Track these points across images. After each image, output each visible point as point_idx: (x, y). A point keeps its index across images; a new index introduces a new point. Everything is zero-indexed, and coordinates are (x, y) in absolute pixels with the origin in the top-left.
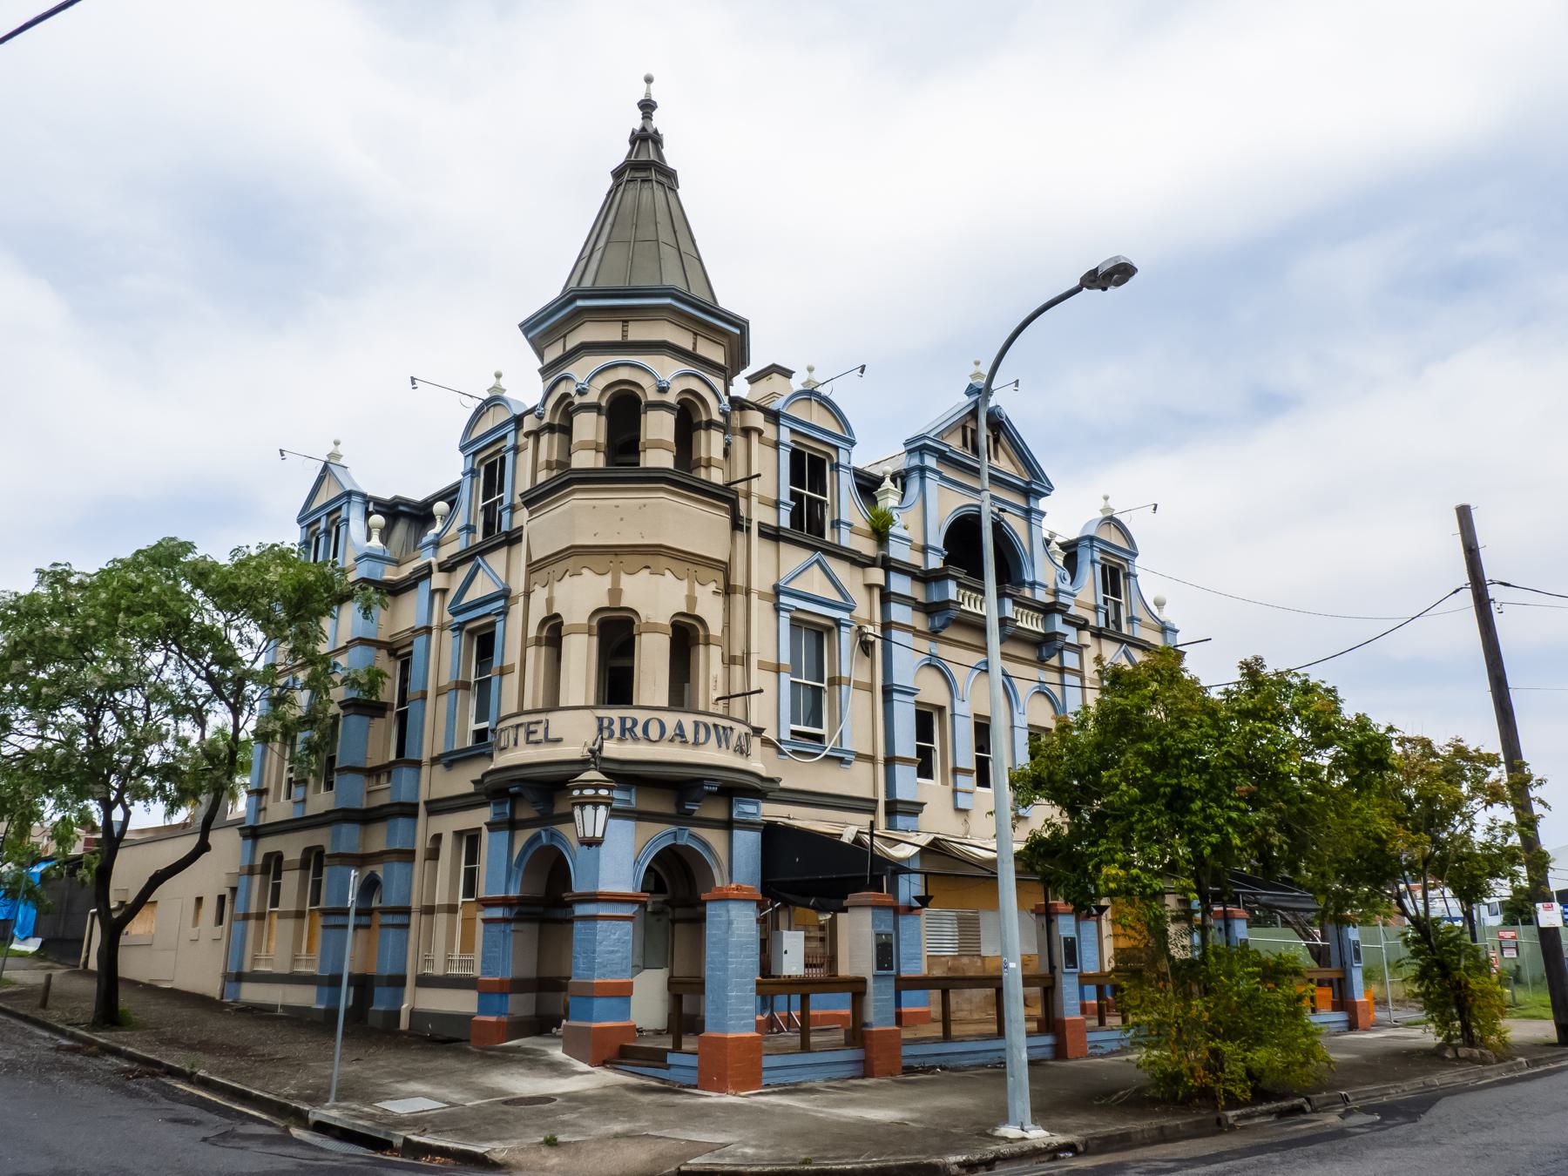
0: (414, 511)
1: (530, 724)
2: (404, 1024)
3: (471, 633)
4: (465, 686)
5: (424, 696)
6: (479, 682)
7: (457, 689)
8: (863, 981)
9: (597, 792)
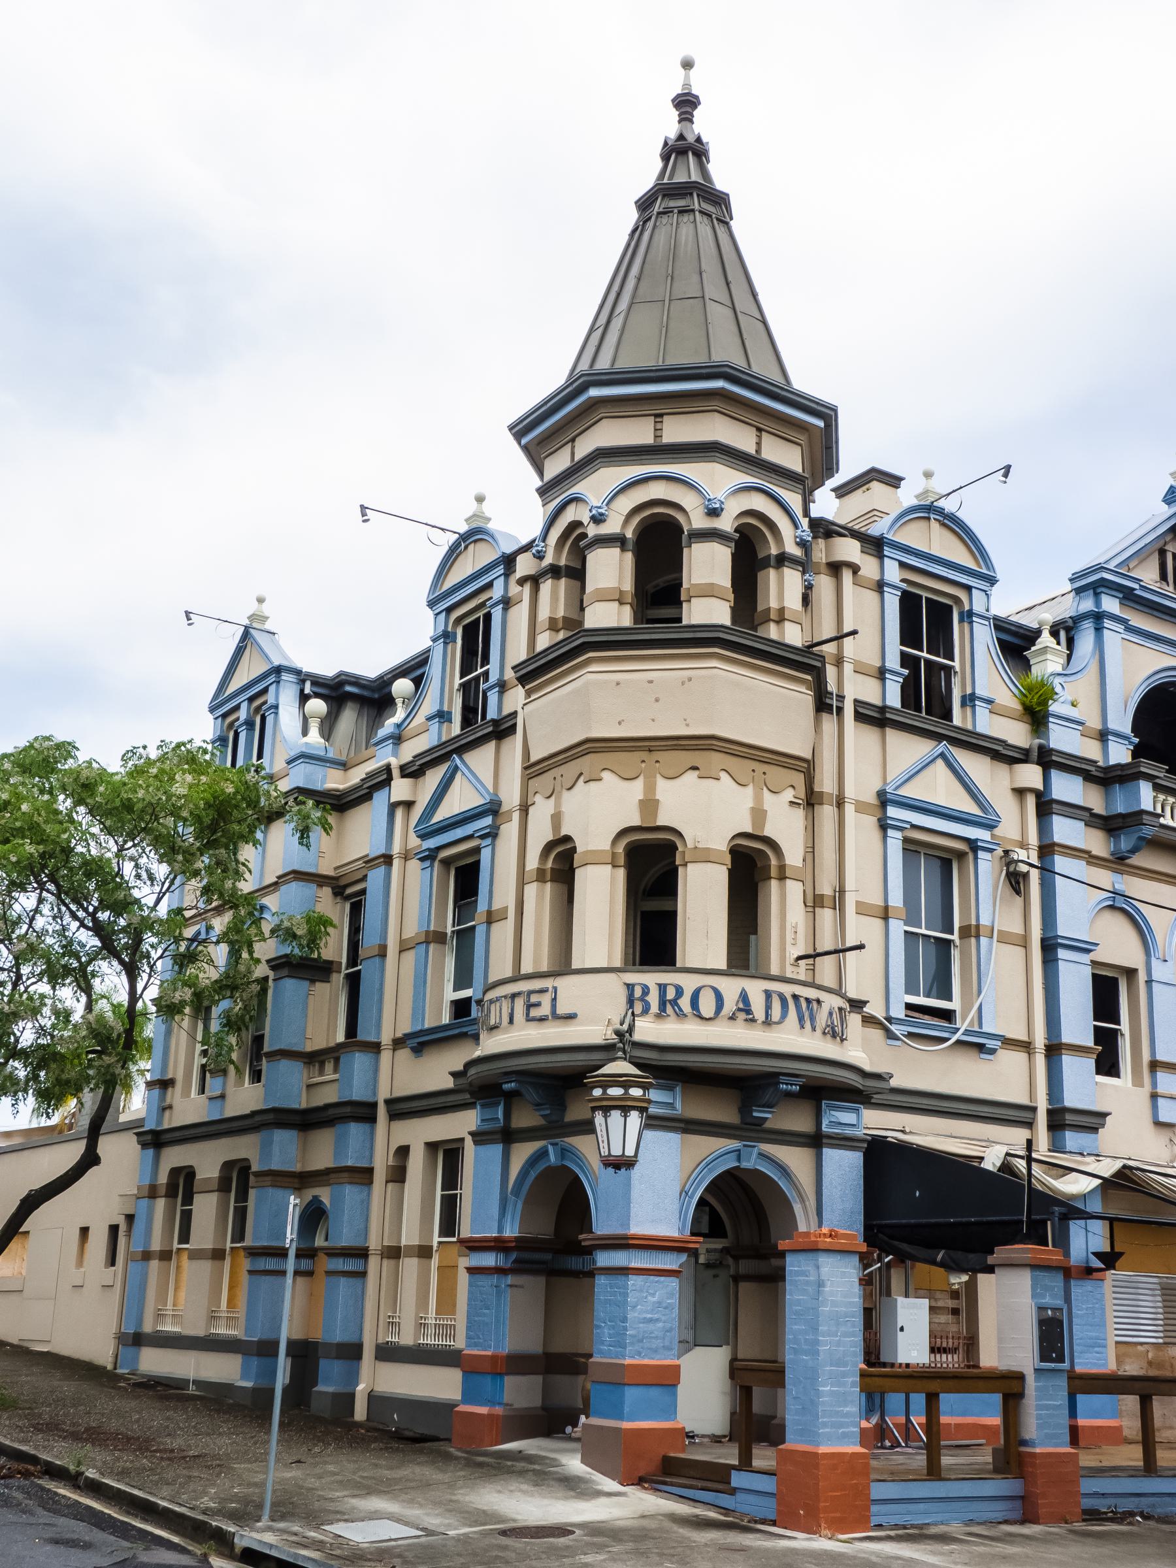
0: (366, 693)
1: (530, 992)
2: (360, 1412)
3: (446, 863)
4: (439, 938)
5: (382, 953)
6: (459, 933)
7: (427, 942)
8: (1020, 1377)
9: (604, 1092)
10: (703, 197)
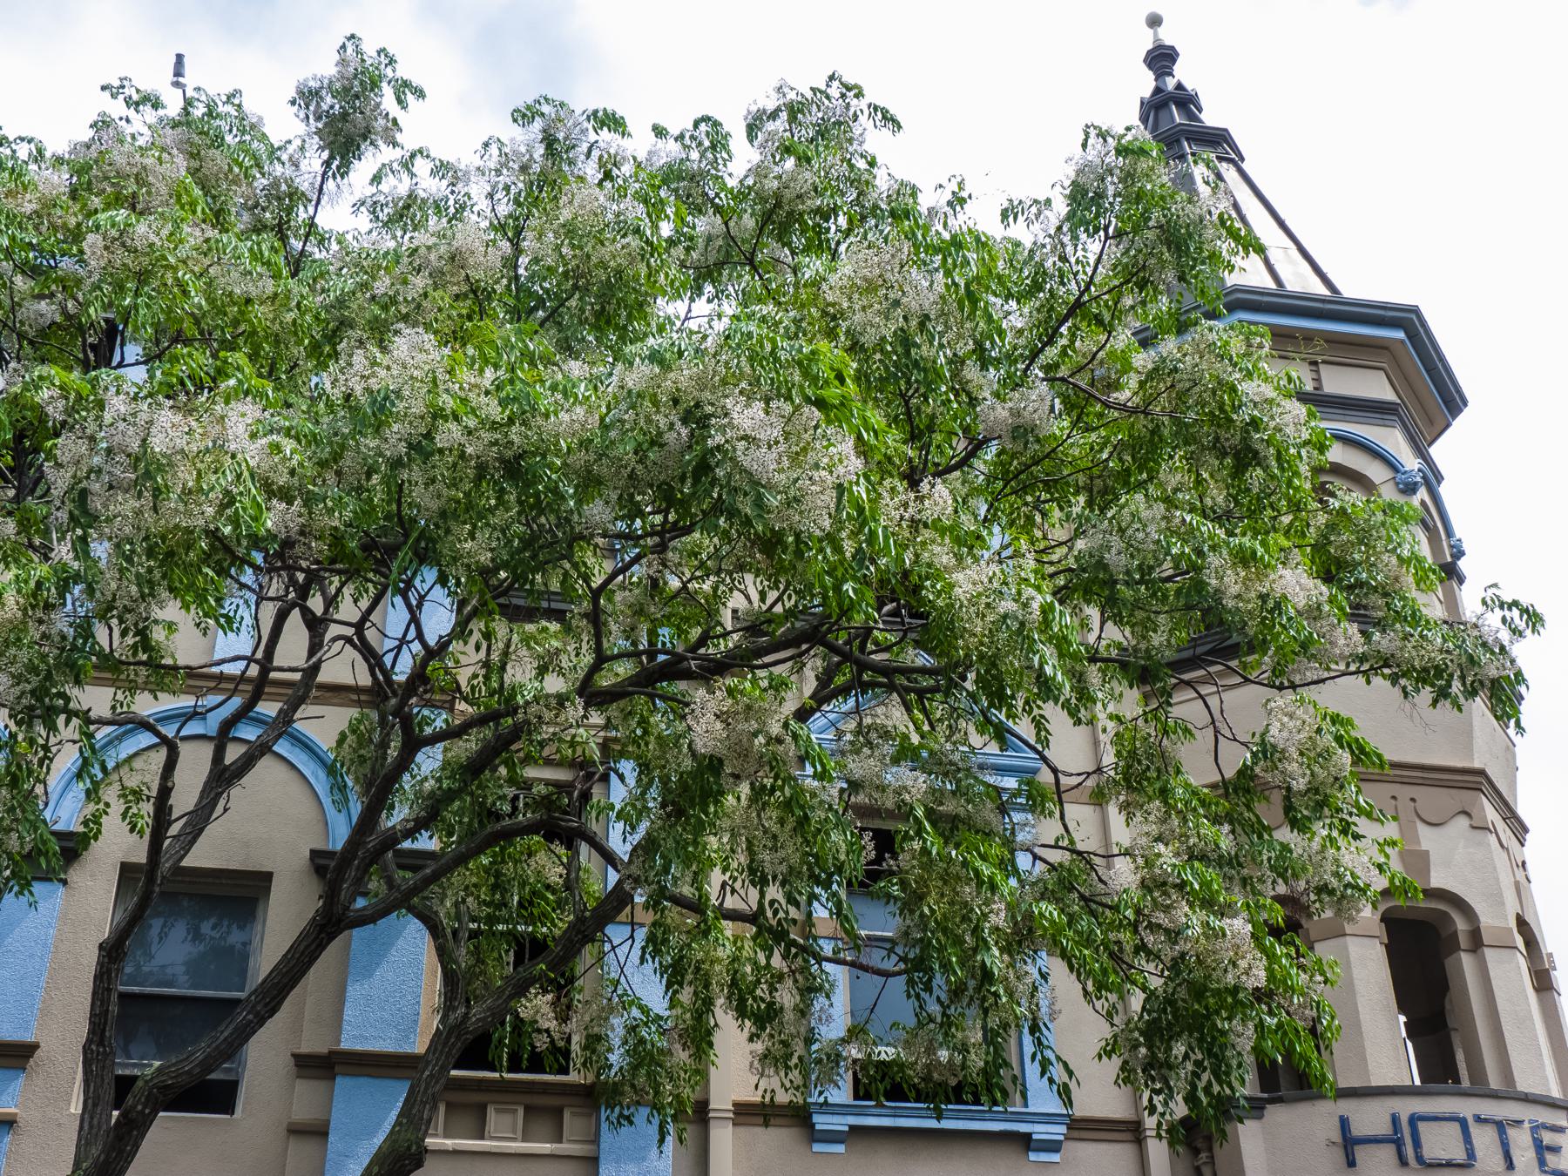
10: (1195, 140)
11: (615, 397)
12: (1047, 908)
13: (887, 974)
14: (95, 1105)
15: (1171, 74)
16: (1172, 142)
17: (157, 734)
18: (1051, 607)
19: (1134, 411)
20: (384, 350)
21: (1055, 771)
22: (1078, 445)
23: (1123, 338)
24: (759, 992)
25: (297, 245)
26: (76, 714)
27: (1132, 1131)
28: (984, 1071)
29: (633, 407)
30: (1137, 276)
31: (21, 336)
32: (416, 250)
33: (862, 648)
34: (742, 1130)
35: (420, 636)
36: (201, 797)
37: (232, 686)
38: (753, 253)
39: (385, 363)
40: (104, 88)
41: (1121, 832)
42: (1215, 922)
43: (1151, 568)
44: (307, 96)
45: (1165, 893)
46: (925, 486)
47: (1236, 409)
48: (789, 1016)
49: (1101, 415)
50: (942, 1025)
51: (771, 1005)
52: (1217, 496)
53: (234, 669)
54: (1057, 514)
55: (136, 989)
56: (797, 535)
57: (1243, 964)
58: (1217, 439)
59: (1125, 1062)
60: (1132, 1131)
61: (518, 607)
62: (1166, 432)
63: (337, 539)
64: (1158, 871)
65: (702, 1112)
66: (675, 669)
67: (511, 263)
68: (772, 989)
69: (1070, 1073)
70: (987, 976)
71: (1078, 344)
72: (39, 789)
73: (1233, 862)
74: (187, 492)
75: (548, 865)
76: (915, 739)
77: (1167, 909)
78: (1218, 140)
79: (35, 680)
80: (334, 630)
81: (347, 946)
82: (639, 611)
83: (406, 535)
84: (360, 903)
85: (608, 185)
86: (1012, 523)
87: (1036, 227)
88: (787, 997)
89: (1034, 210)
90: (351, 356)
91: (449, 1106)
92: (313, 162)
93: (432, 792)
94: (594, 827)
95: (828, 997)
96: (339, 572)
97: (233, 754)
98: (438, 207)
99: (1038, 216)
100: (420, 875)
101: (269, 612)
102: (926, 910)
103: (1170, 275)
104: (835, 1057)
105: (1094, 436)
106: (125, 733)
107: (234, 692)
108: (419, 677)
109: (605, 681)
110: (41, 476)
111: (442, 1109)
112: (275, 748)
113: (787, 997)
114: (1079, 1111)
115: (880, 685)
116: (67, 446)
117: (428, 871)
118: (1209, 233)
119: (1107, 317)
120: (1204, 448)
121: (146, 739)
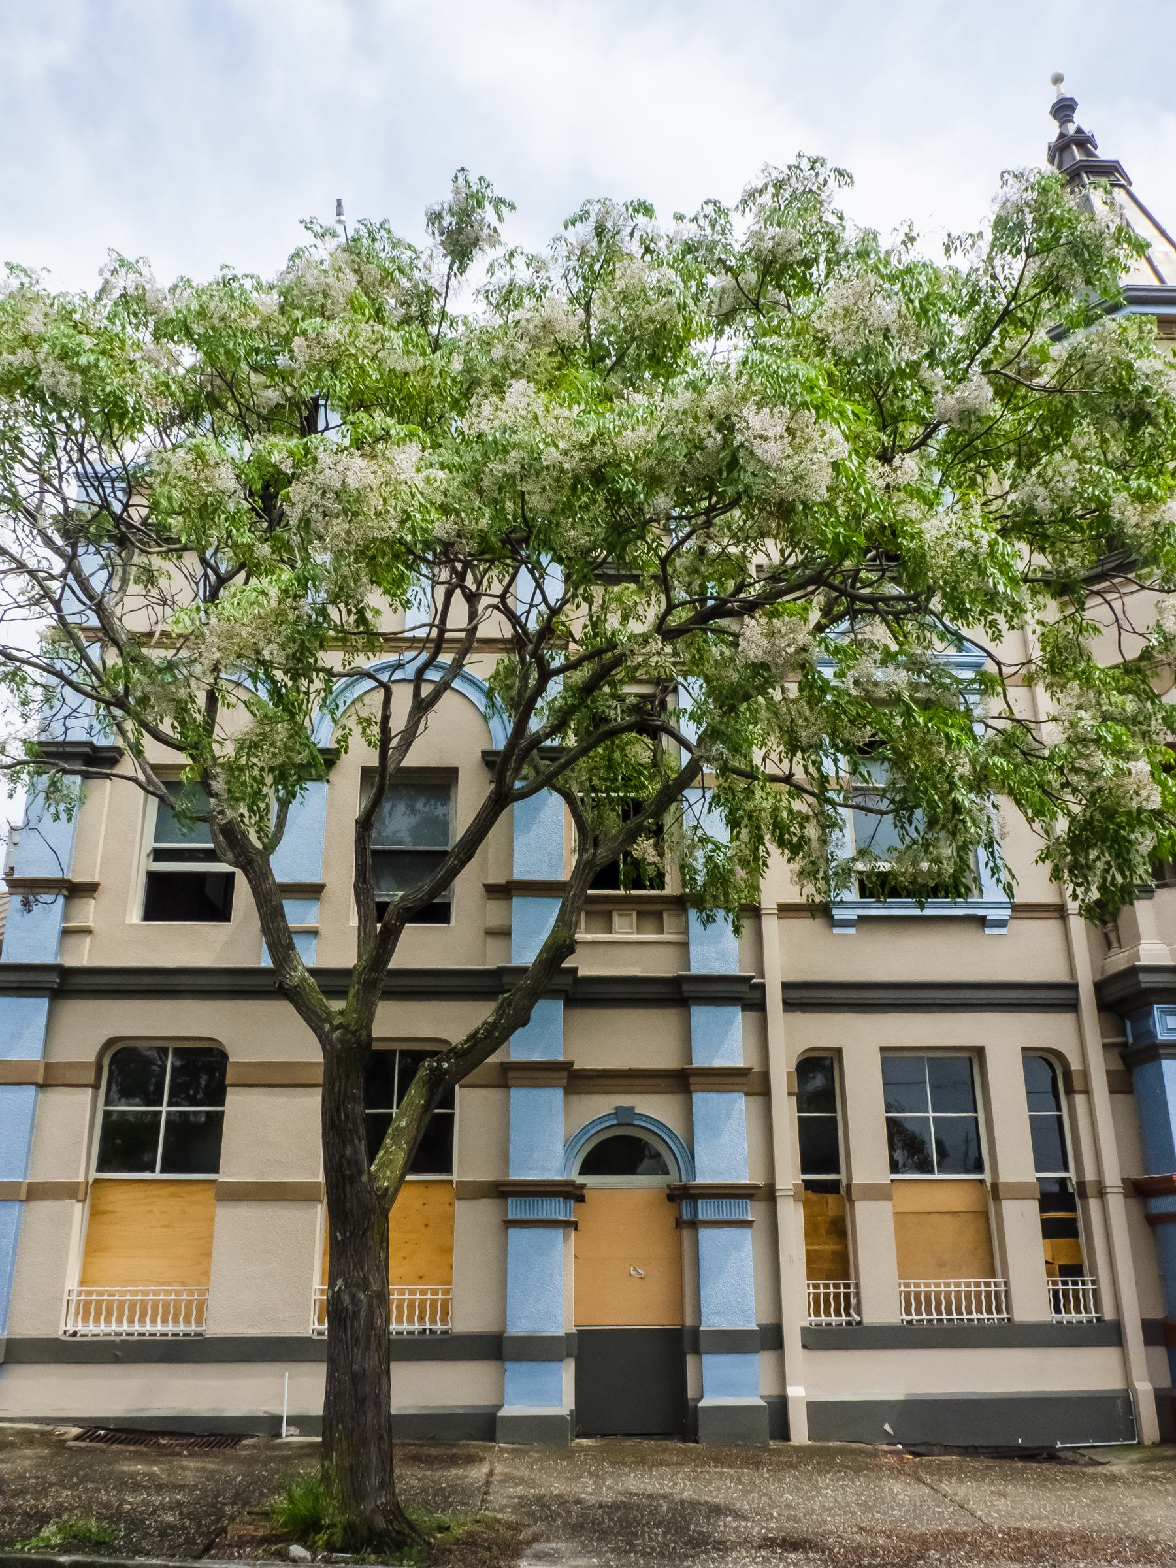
10: (1092, 172)
11: (667, 417)
12: (998, 760)
13: (882, 813)
14: (366, 921)
15: (1072, 121)
16: (1074, 176)
17: (376, 680)
18: (996, 542)
19: (1051, 391)
20: (503, 399)
21: (998, 664)
22: (1008, 422)
23: (1041, 336)
24: (792, 829)
25: (433, 329)
26: (323, 670)
27: (1059, 911)
28: (954, 876)
29: (680, 422)
30: (1052, 284)
31: (259, 416)
32: (519, 322)
33: (853, 586)
34: (783, 921)
35: (545, 600)
36: (409, 720)
37: (421, 645)
38: (758, 301)
39: (504, 408)
40: (301, 222)
41: (1046, 703)
42: (1123, 765)
43: (1070, 509)
44: (435, 217)
45: (1085, 746)
46: (897, 461)
47: (1131, 381)
48: (815, 844)
49: (1025, 397)
50: (922, 845)
51: (802, 837)
52: (1116, 450)
53: (422, 633)
54: (993, 475)
55: (380, 847)
56: (804, 503)
57: (1144, 793)
58: (1117, 407)
59: (1056, 865)
60: (1059, 911)
61: (610, 576)
62: (1076, 405)
63: (483, 537)
64: (1080, 730)
65: (755, 912)
66: (721, 610)
67: (585, 325)
68: (802, 827)
69: (1013, 877)
70: (957, 808)
71: (1007, 343)
72: (307, 723)
73: (1134, 720)
74: (378, 514)
75: (640, 750)
76: (894, 647)
77: (1087, 757)
78: (1110, 171)
79: (295, 647)
80: (484, 601)
81: (511, 815)
82: (694, 571)
83: (530, 532)
84: (518, 785)
85: (648, 257)
86: (960, 485)
87: (972, 255)
88: (812, 831)
89: (970, 242)
90: (479, 406)
91: (587, 913)
92: (441, 265)
93: (561, 707)
94: (672, 723)
95: (841, 830)
96: (486, 561)
97: (426, 690)
98: (530, 290)
99: (972, 247)
100: (557, 764)
101: (441, 591)
102: (913, 766)
103: (1079, 281)
104: (847, 871)
105: (1021, 413)
106: (356, 680)
107: (423, 648)
108: (547, 630)
109: (673, 621)
110: (283, 514)
111: (583, 915)
112: (453, 685)
113: (812, 831)
114: (1018, 899)
115: (867, 611)
116: (296, 491)
117: (562, 760)
118: (1108, 243)
119: (1028, 318)
120: (1107, 414)
121: (369, 684)
